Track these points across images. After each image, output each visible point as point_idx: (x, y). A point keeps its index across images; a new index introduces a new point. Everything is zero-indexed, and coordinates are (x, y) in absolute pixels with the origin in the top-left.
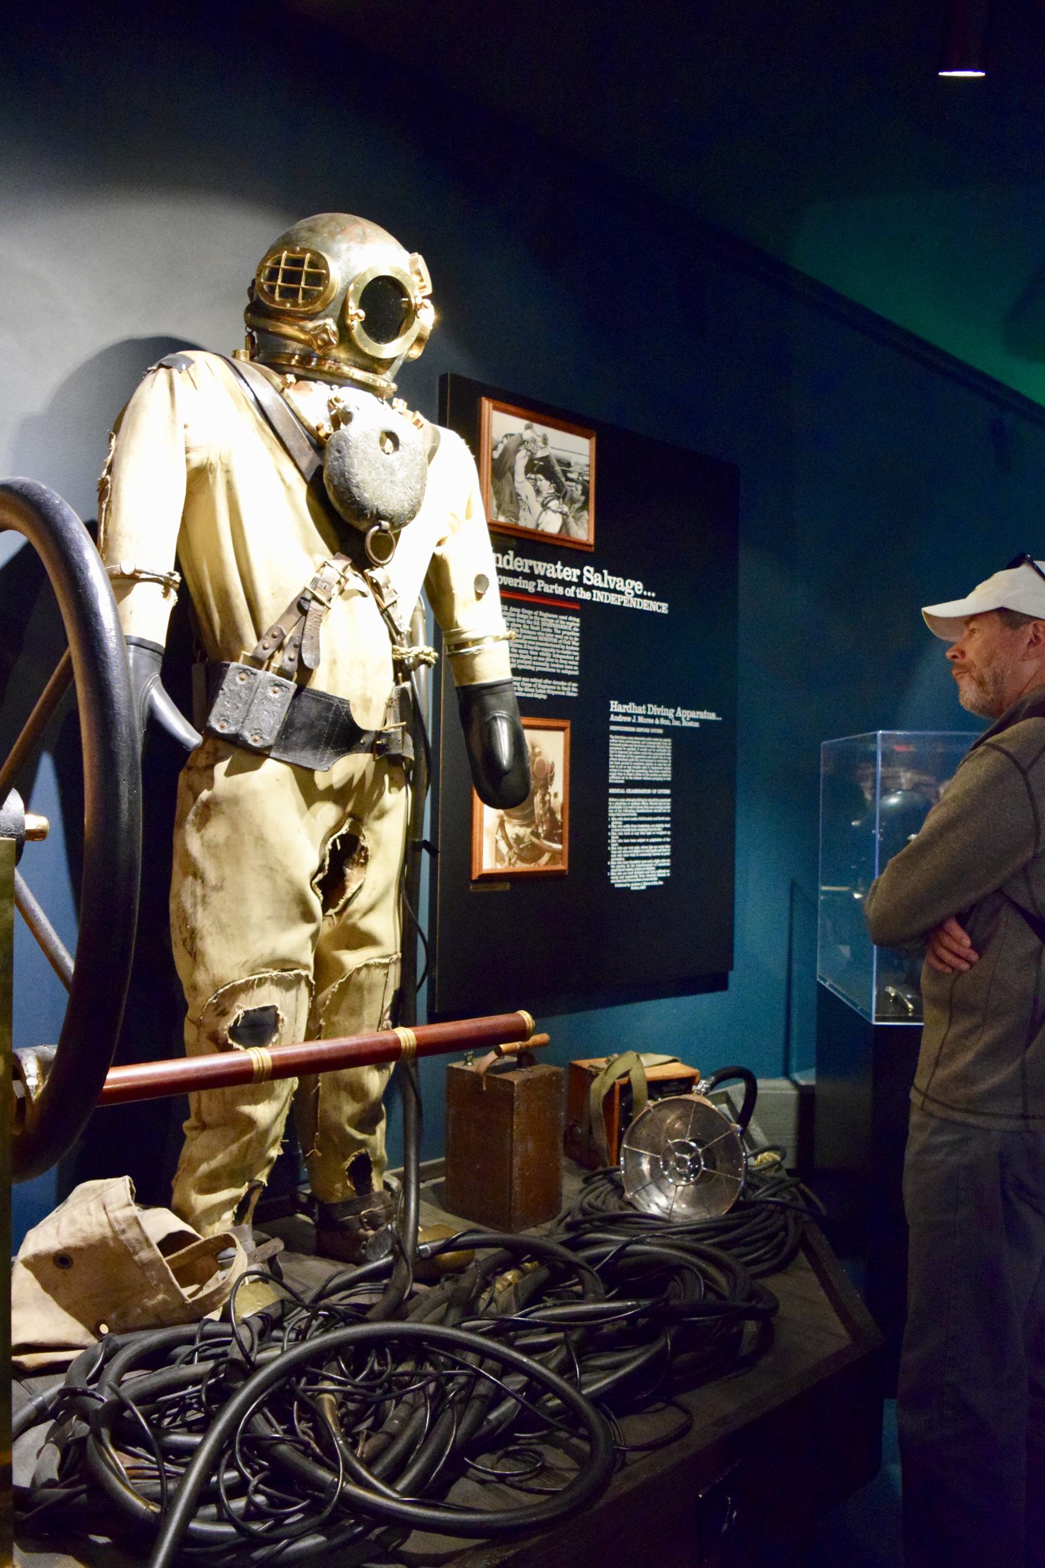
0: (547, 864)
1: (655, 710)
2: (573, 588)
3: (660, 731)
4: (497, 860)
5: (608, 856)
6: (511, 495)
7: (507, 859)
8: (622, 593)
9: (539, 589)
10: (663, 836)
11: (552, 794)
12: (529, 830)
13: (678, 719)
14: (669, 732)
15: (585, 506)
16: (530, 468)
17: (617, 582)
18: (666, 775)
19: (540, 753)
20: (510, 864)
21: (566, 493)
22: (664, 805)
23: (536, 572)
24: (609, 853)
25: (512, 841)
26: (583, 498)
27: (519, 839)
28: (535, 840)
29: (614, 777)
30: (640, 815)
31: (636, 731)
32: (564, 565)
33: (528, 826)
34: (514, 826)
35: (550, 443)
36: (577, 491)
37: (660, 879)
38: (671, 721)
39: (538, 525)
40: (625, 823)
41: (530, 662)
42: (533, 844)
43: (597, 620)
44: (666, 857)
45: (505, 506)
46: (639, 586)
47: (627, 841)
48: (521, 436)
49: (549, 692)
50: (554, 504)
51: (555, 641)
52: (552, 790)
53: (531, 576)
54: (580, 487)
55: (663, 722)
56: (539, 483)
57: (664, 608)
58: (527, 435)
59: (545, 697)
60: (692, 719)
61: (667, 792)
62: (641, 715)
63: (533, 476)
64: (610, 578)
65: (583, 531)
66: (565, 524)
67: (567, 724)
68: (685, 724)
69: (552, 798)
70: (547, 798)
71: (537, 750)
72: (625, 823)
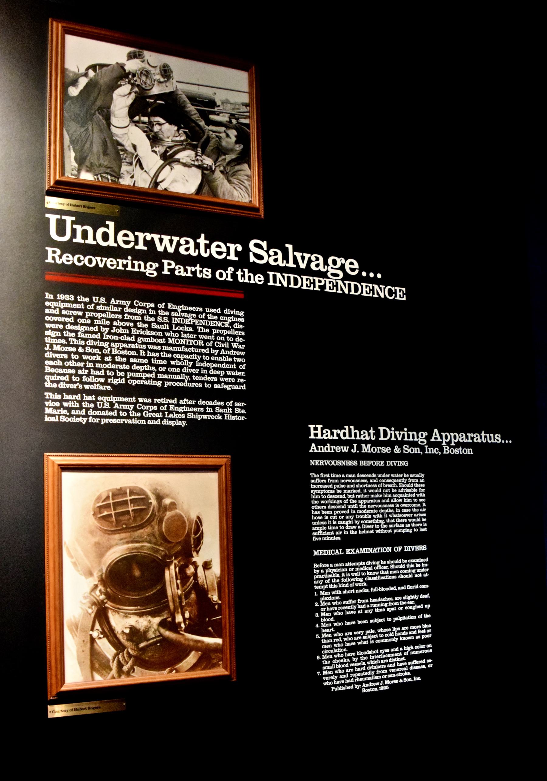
0: (193, 668)
1: (392, 434)
2: (230, 270)
3: (404, 463)
4: (93, 668)
5: (317, 647)
6: (105, 144)
7: (114, 666)
8: (324, 275)
9: (166, 272)
10: (417, 612)
11: (200, 563)
12: (156, 620)
13: (438, 445)
14: (417, 464)
15: (243, 158)
16: (137, 109)
17: (317, 262)
18: (419, 523)
19: (173, 505)
20: (120, 671)
21: (208, 139)
22: (420, 567)
23: (160, 249)
24: (319, 643)
25: (123, 639)
26: (239, 148)
27: (135, 634)
28: (167, 633)
29: (319, 533)
30: (371, 584)
31: (354, 466)
32: (211, 239)
33: (153, 614)
34: (126, 615)
35: (176, 76)
36: (230, 138)
37: (414, 673)
38: (422, 448)
39: (157, 184)
40: (344, 597)
41: (153, 375)
42: (164, 640)
43: (272, 315)
44: (425, 642)
45: (92, 158)
46: (352, 265)
47: (345, 624)
48: (122, 66)
49: (190, 416)
50: (186, 155)
51: (201, 343)
52: (199, 559)
53: (151, 254)
54: (233, 133)
55: (407, 450)
56: (156, 128)
57: (401, 294)
58: (132, 66)
59: (183, 424)
60: (458, 445)
61: (423, 548)
62: (366, 442)
63: (145, 119)
64: (298, 255)
65: (242, 190)
66: (207, 182)
67: (222, 460)
68: (447, 451)
69: (200, 570)
70: (191, 570)
71: (167, 501)
72: (344, 597)
